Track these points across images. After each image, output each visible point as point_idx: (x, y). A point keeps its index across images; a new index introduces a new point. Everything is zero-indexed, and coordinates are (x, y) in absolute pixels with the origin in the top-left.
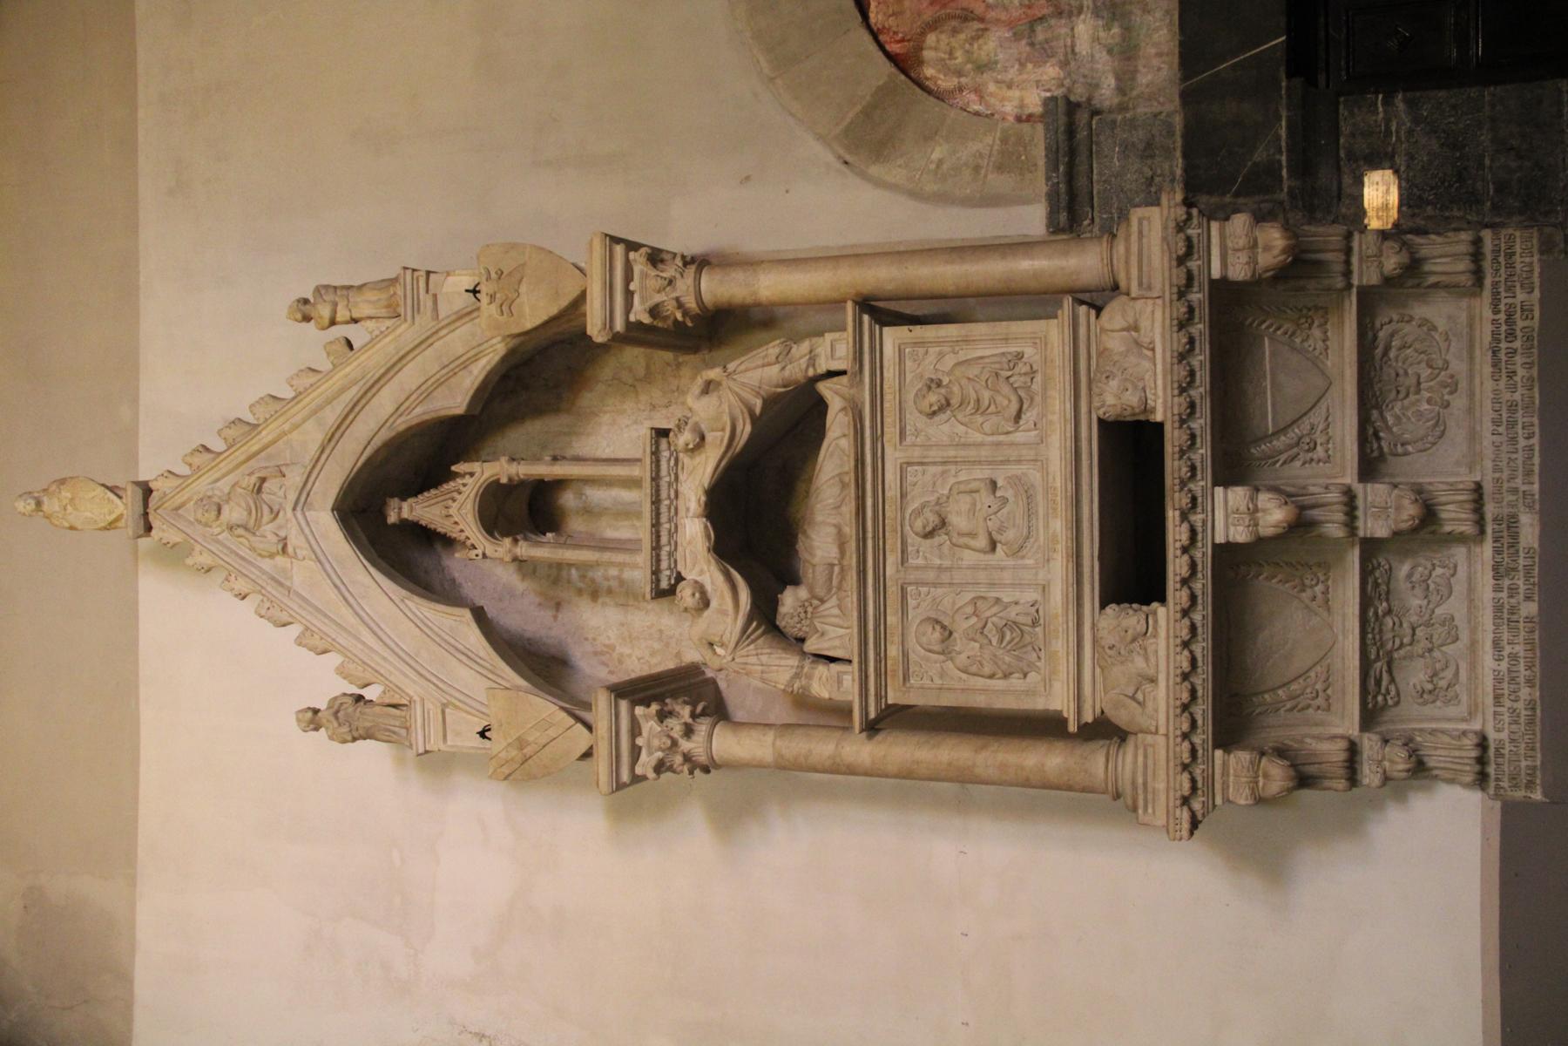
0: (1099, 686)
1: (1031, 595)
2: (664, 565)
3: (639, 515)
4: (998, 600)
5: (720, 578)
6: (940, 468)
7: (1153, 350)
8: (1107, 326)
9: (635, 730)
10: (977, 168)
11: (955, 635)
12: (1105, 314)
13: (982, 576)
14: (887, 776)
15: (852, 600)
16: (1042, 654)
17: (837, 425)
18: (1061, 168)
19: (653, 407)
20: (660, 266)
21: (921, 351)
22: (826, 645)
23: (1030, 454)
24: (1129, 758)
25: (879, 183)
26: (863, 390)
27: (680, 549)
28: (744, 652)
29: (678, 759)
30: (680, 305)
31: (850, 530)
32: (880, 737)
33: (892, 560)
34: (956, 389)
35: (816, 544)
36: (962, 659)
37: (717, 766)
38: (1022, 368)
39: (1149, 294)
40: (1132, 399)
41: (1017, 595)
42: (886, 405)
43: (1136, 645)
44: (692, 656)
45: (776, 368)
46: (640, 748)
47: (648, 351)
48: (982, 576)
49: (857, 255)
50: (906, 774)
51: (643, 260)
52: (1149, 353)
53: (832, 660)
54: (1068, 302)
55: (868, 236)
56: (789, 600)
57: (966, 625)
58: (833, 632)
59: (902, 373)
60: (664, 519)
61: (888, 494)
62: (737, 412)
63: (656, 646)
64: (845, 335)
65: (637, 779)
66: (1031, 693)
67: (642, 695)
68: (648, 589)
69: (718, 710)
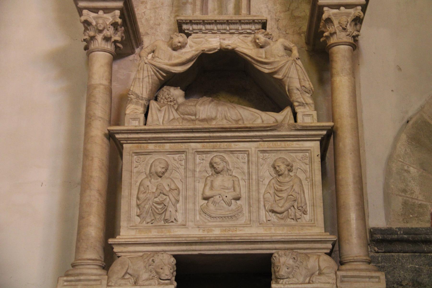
0: (133, 255)
1: (180, 218)
2: (195, 27)
3: (220, 13)
4: (178, 201)
5: (188, 56)
6: (246, 171)
7: (309, 283)
8: (321, 259)
9: (107, 10)
10: (405, 191)
11: (160, 179)
12: (327, 257)
13: (190, 193)
14: (85, 143)
15: (177, 125)
18: (405, 236)
19: (278, 21)
20: (353, 23)
21: (307, 161)
22: (154, 112)
24: (95, 271)
25: (397, 139)
26: (288, 131)
27: (204, 35)
28: (150, 69)
29: (92, 33)
30: (332, 34)
32: (105, 140)
33: (199, 146)
34: (287, 179)
35: (206, 106)
36: (147, 182)
37: (88, 55)
39: (338, 280)
40: (283, 271)
41: (180, 211)
42: (279, 143)
43: (155, 274)
44: (147, 41)
45: (298, 86)
46: (97, 13)
47: (308, 18)
48: (190, 193)
49: (357, 128)
50: (86, 154)
51: (357, 14)
52: (307, 280)
53: (146, 115)
55: (367, 133)
56: (177, 93)
58: (161, 115)
59: (296, 151)
60: (219, 26)
61: (233, 144)
62: (275, 65)
63: (152, 22)
65: (80, 11)
66: (129, 219)
67: (126, 14)
68: (182, 18)
69: (119, 53)
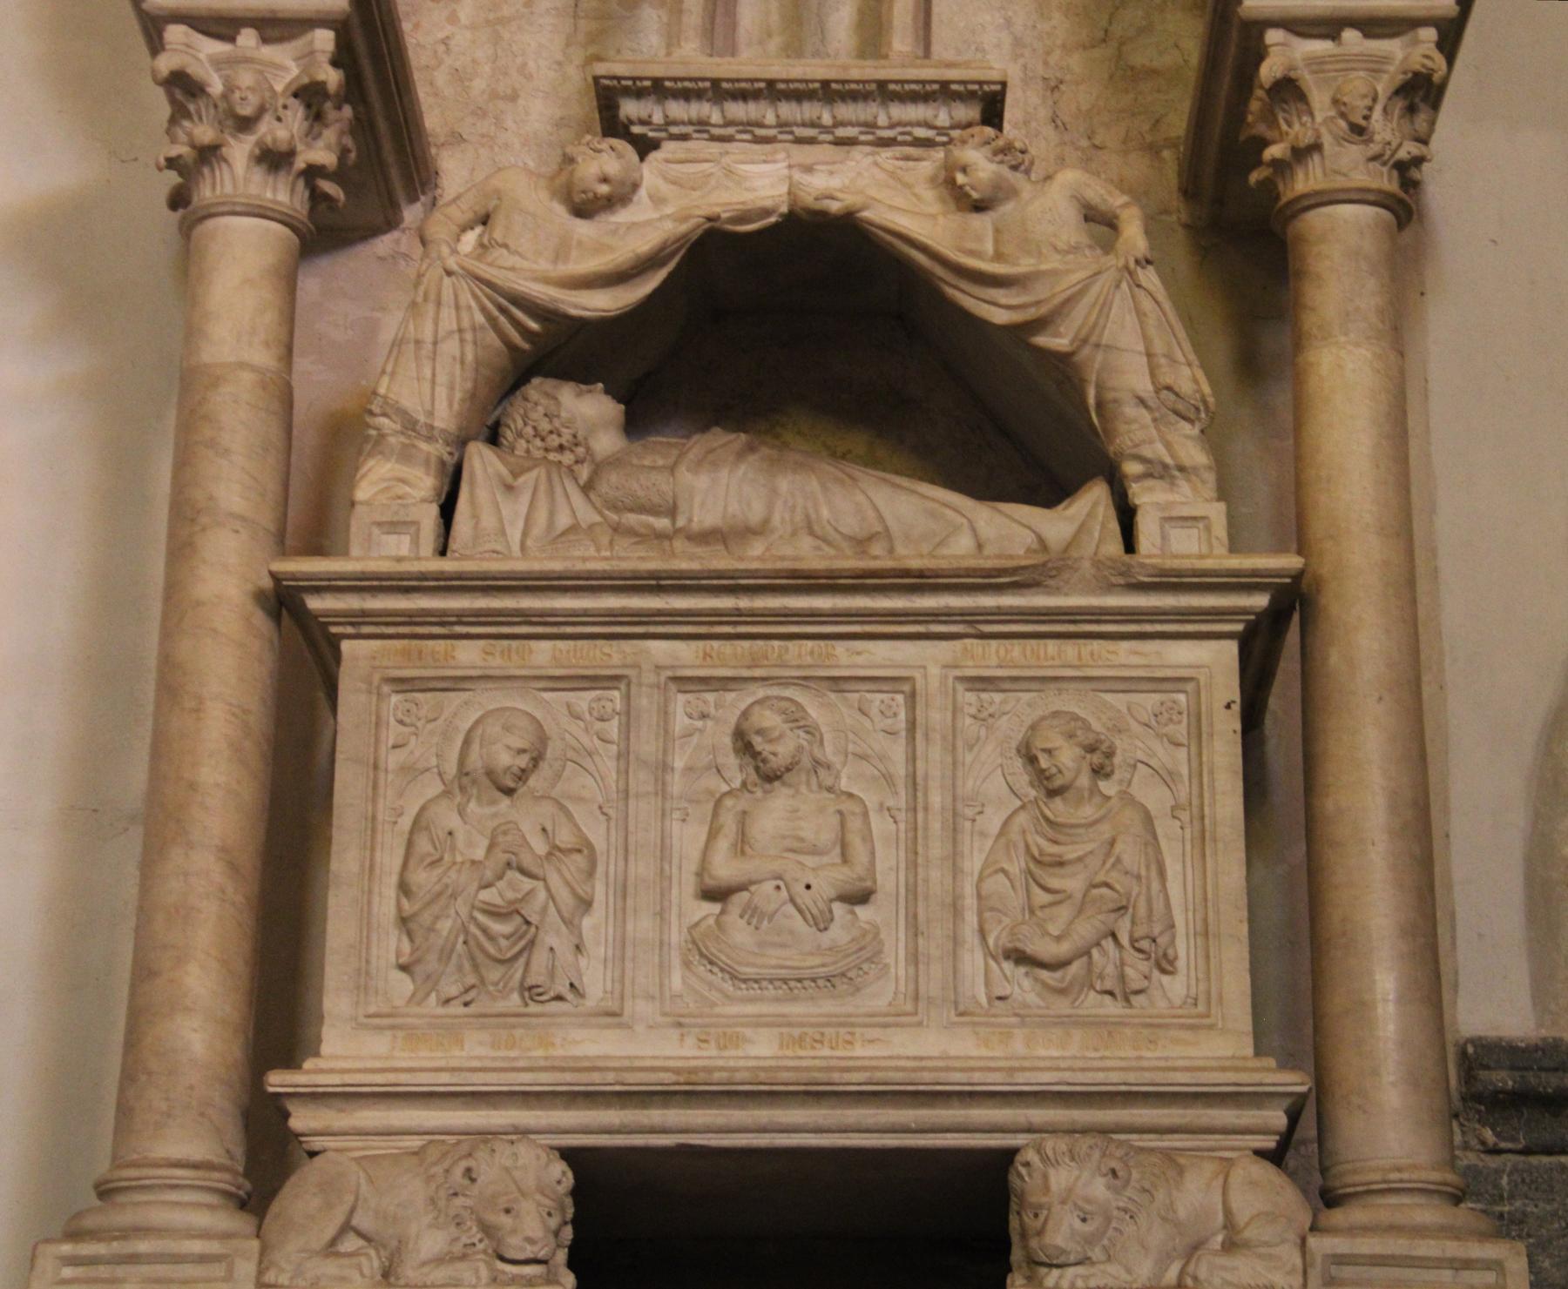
0: (380, 1146)
1: (596, 982)
2: (677, 109)
4: (586, 904)
5: (644, 244)
8: (1237, 1176)
11: (505, 803)
12: (1265, 1172)
13: (642, 868)
15: (588, 558)
16: (456, 1009)
17: (1003, 529)
19: (1055, 88)
20: (1399, 105)
21: (1180, 731)
22: (483, 495)
23: (933, 984)
24: (202, 1219)
26: (1092, 592)
27: (715, 148)
28: (466, 298)
29: (205, 133)
30: (1301, 154)
31: (755, 556)
32: (261, 620)
33: (685, 655)
34: (1088, 812)
35: (724, 474)
38: (1136, 969)
40: (1062, 1231)
41: (597, 950)
42: (1052, 646)
44: (455, 172)
45: (1144, 386)
46: (232, 39)
47: (1191, 76)
48: (642, 868)
49: (1411, 583)
50: (172, 684)
51: (1417, 63)
53: (447, 511)
54: (1296, 1082)
55: (1456, 608)
56: (589, 410)
57: (529, 828)
58: (514, 511)
59: (1129, 684)
60: (788, 110)
61: (840, 647)
62: (1040, 291)
63: (479, 85)
64: (1221, 550)
66: (363, 982)
68: (620, 69)
